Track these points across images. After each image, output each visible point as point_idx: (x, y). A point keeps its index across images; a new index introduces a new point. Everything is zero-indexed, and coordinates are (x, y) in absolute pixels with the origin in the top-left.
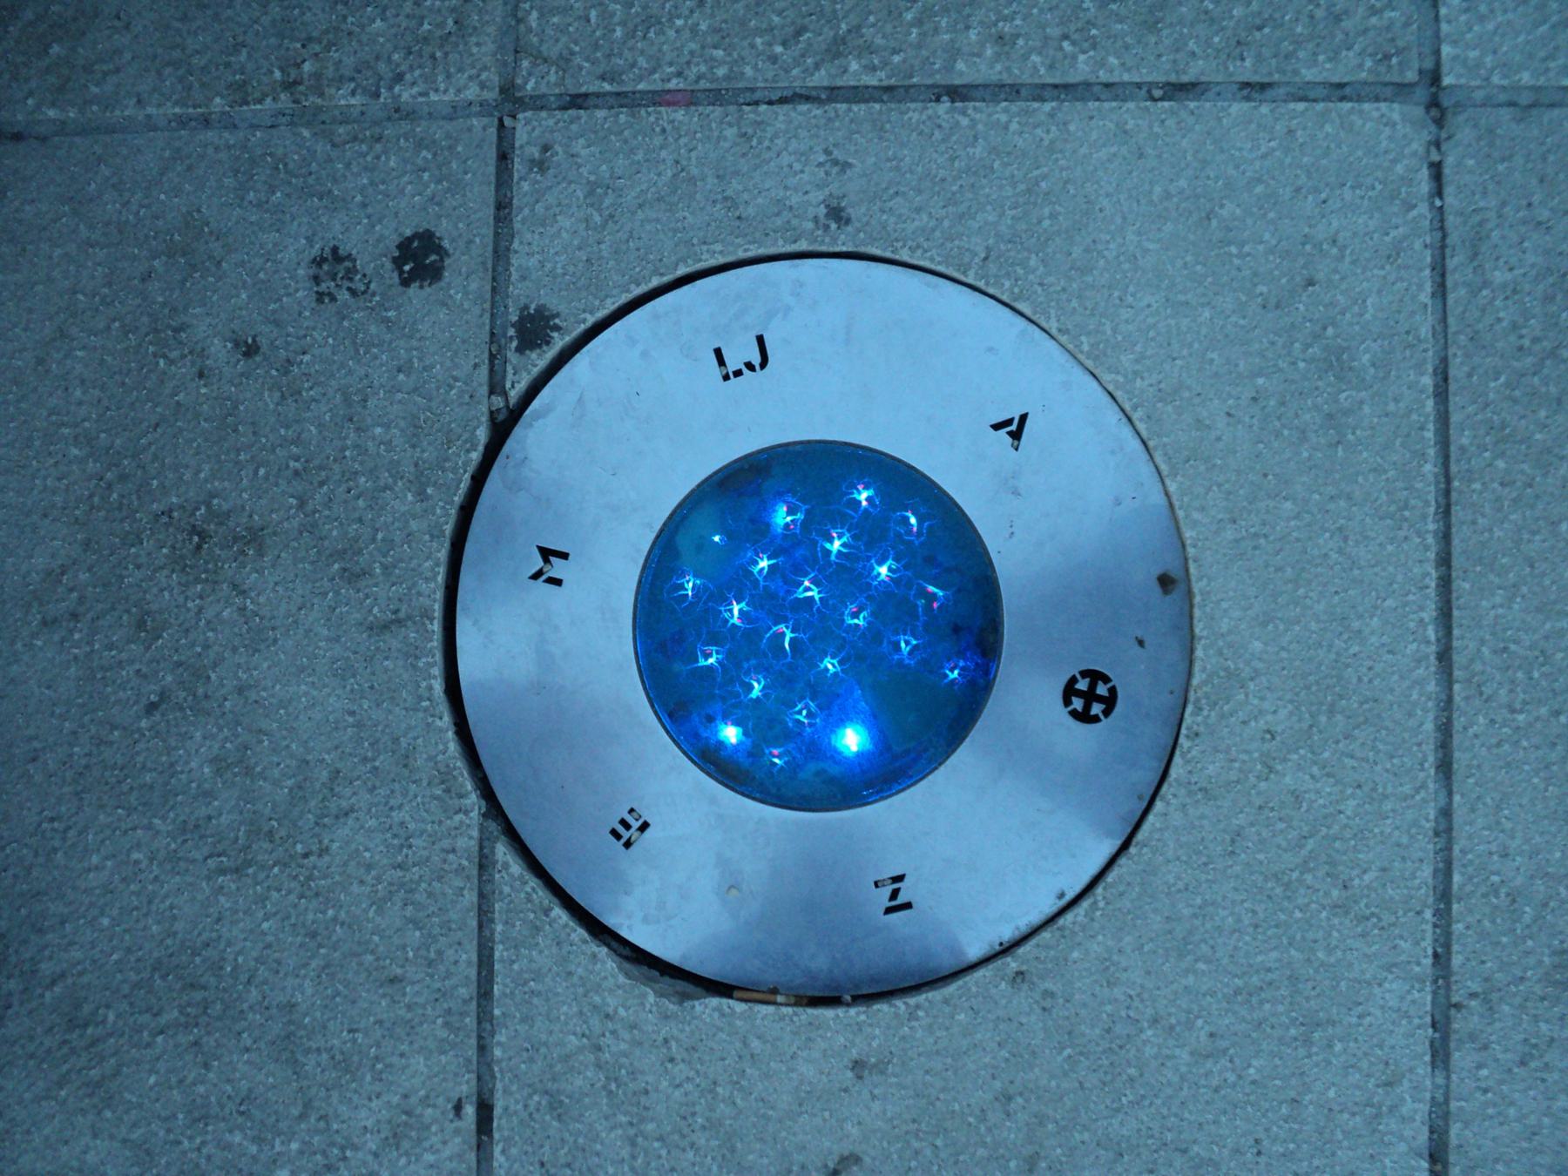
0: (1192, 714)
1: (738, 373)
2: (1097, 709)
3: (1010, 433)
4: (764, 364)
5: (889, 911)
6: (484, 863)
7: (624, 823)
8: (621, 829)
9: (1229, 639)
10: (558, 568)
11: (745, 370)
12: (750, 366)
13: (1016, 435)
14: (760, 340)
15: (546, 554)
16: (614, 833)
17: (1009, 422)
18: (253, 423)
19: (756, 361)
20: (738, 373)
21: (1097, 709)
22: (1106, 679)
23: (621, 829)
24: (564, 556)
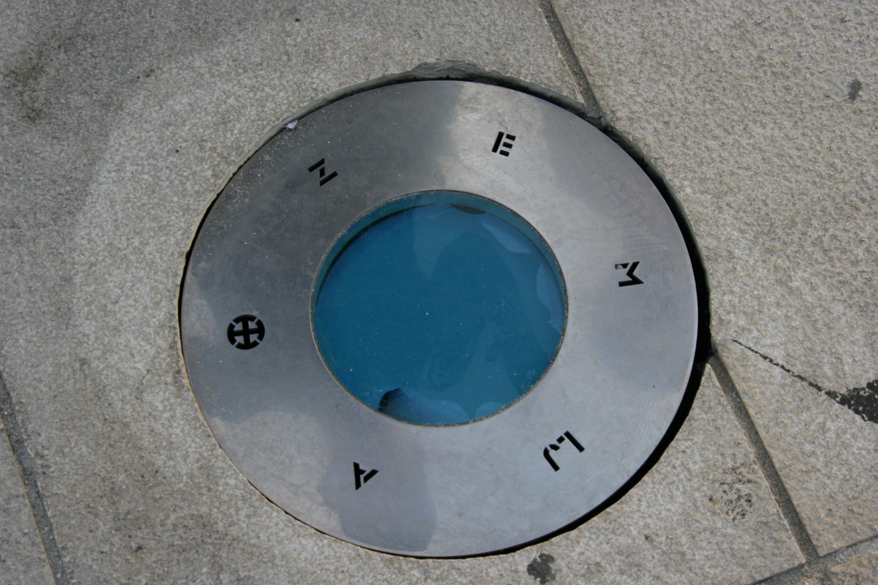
0: (175, 342)
1: (561, 440)
2: (240, 339)
3: (363, 472)
4: (546, 453)
5: (322, 183)
6: (588, 91)
7: (510, 146)
8: (506, 149)
9: (41, 156)
10: (565, 454)
11: (557, 443)
12: (555, 447)
13: (358, 471)
14: (556, 468)
15: (636, 281)
16: (512, 138)
17: (366, 479)
18: (777, 412)
19: (552, 453)
20: (561, 440)
21: (240, 339)
22: (240, 346)
23: (506, 149)
24: (622, 284)
